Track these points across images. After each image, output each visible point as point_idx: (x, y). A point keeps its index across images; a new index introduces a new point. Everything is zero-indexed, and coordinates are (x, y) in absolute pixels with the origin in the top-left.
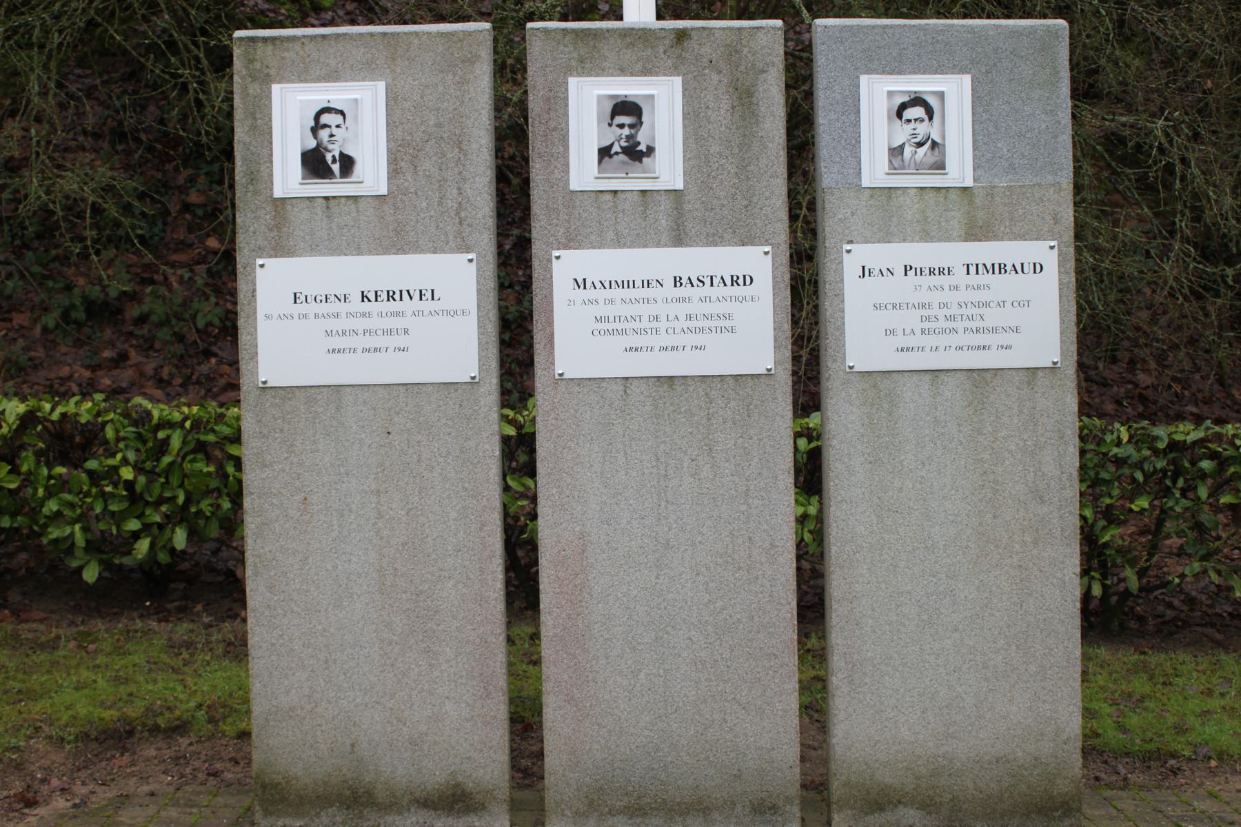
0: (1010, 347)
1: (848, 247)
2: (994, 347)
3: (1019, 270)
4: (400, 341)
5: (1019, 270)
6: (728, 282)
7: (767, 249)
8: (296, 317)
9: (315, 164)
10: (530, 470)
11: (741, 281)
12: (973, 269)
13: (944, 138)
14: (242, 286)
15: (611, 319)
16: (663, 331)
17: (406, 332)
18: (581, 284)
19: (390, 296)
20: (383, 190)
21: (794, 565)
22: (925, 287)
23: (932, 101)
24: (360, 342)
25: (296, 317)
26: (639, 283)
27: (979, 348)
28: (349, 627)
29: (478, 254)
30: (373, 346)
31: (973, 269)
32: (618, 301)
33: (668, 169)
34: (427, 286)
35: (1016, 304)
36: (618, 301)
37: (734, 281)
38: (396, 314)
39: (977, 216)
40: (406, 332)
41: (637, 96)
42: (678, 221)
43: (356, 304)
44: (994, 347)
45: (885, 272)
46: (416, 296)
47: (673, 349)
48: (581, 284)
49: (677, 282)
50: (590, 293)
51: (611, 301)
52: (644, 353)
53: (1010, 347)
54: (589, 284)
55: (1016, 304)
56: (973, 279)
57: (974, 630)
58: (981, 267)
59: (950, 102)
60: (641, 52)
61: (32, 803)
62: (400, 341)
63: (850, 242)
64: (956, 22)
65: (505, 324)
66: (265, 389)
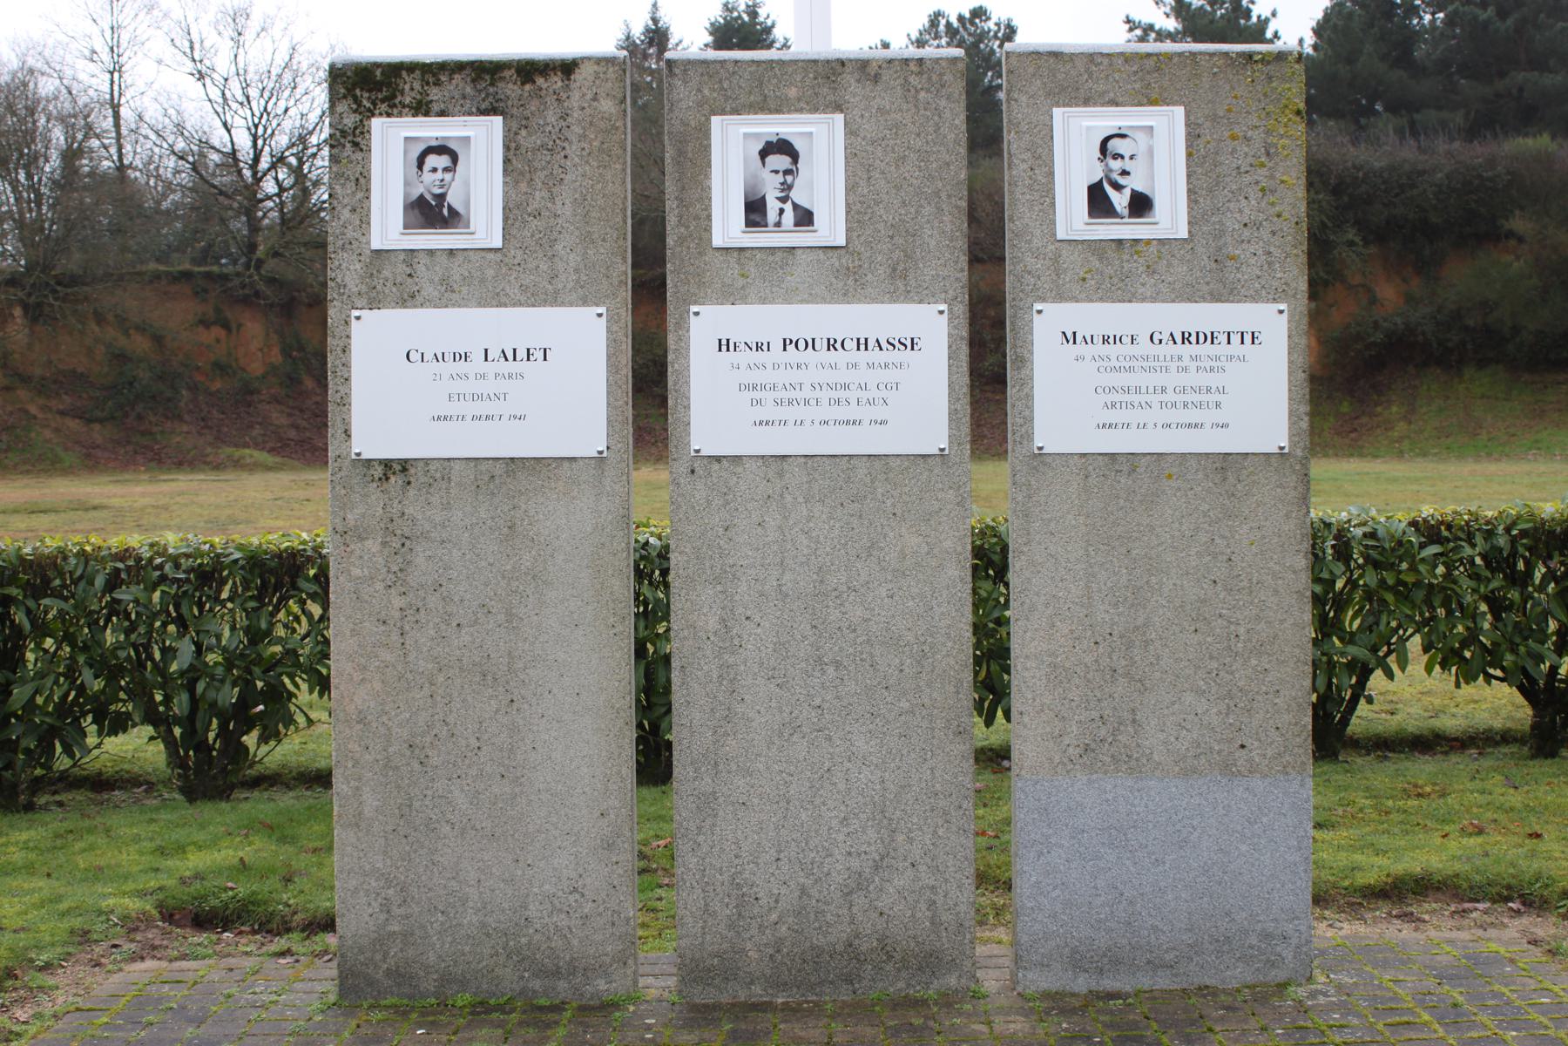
3: (510, 357)
4: (878, 412)
5: (510, 357)
6: (1179, 339)
7: (1283, 307)
8: (472, 377)
9: (1098, 202)
10: (1001, 574)
11: (1193, 339)
12: (1248, 338)
13: (1153, 188)
15: (1144, 390)
16: (854, 402)
17: (1218, 405)
18: (724, 345)
19: (1105, 340)
21: (1308, 653)
22: (446, 376)
23: (798, 145)
25: (472, 377)
26: (522, 354)
27: (848, 422)
28: (463, 780)
29: (950, 310)
30: (484, 414)
31: (1248, 338)
32: (863, 366)
34: (537, 343)
36: (863, 366)
39: (1205, 269)
40: (1218, 405)
43: (1144, 347)
44: (866, 422)
47: (487, 417)
48: (724, 345)
51: (855, 366)
52: (453, 423)
54: (1079, 338)
57: (1177, 817)
59: (1161, 143)
61: (100, 869)
62: (878, 412)
66: (1040, 455)
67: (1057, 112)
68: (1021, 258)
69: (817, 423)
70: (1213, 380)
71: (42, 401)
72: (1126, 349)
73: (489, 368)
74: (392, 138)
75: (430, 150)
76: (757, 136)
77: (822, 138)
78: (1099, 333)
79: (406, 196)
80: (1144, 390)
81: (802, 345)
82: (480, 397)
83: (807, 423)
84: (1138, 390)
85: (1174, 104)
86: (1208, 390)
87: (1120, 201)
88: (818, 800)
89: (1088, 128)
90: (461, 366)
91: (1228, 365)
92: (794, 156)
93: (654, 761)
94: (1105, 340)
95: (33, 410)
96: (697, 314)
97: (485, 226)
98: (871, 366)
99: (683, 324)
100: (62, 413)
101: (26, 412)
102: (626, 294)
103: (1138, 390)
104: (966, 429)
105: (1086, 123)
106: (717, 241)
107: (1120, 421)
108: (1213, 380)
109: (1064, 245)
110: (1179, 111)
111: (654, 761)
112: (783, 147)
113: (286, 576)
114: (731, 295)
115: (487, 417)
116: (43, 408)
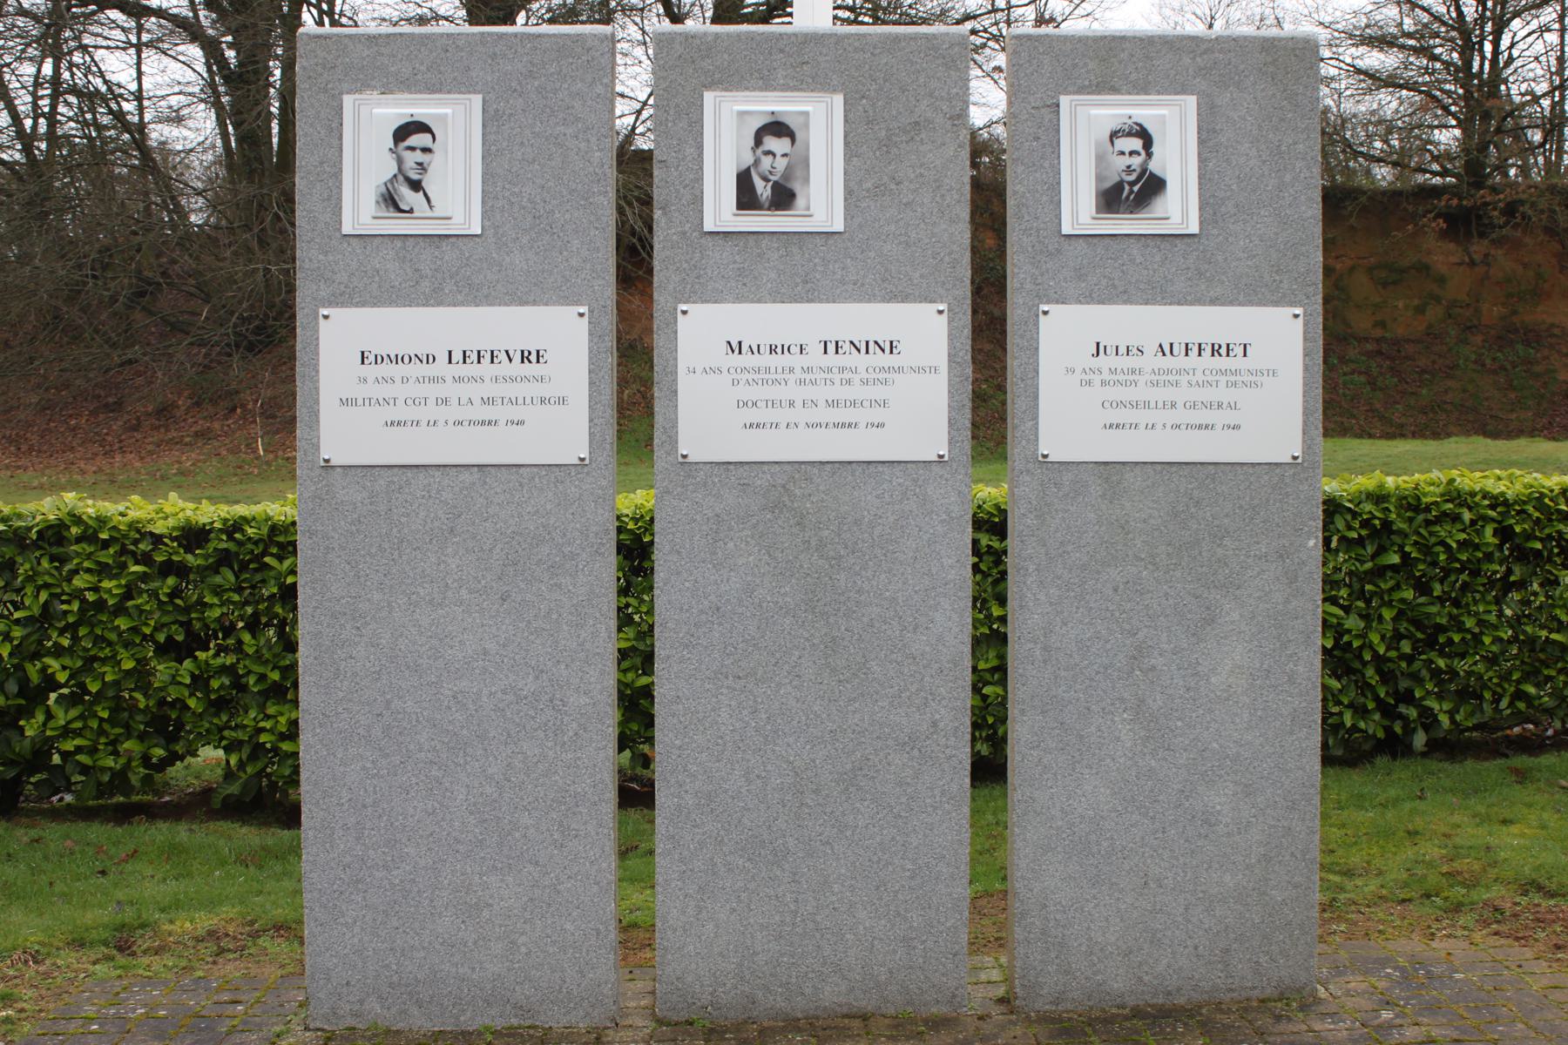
0: (523, 423)
1: (684, 307)
2: (502, 423)
3: (1167, 350)
4: (877, 415)
5: (1167, 350)
7: (1298, 311)
11: (779, 350)
12: (831, 348)
14: (659, 341)
19: (772, 350)
24: (800, 415)
25: (449, 379)
27: (483, 423)
28: (430, 778)
29: (591, 311)
31: (831, 348)
33: (823, 204)
34: (1134, 343)
35: (410, 402)
37: (525, 357)
38: (433, 380)
41: (786, 113)
42: (806, 270)
43: (1151, 361)
50: (747, 360)
52: (408, 429)
53: (523, 423)
54: (745, 348)
55: (410, 402)
56: (832, 359)
60: (808, 63)
62: (877, 415)
63: (1048, 302)
64: (745, 27)
65: (979, 398)
66: (328, 466)
67: (709, 97)
69: (451, 423)
70: (878, 392)
72: (794, 360)
77: (1175, 122)
78: (765, 342)
79: (1099, 178)
80: (1153, 405)
83: (1159, 426)
84: (1147, 405)
87: (763, 190)
89: (742, 114)
91: (1265, 379)
93: (989, 769)
94: (772, 350)
98: (458, 380)
102: (965, 290)
103: (1147, 405)
104: (610, 434)
105: (1094, 111)
106: (347, 228)
107: (768, 420)
108: (878, 392)
109: (354, 241)
110: (1192, 101)
111: (989, 769)
112: (777, 128)
114: (746, 288)
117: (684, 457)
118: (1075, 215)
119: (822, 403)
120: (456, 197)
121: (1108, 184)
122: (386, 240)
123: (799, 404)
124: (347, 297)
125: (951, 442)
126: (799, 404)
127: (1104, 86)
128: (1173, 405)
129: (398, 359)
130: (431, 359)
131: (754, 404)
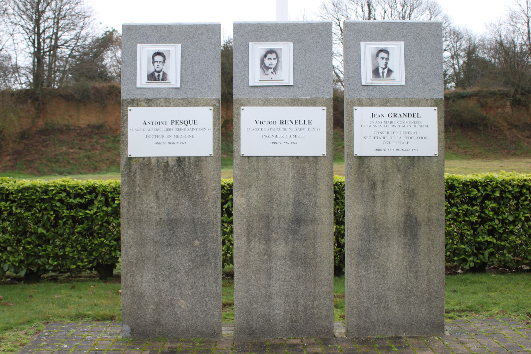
2: (290, 143)
7: (324, 108)
8: (260, 129)
9: (376, 72)
20: (178, 86)
23: (165, 54)
24: (284, 140)
25: (260, 129)
32: (294, 129)
36: (294, 129)
45: (381, 116)
46: (151, 123)
47: (173, 143)
49: (281, 122)
51: (264, 129)
52: (277, 145)
58: (294, 123)
63: (355, 106)
67: (362, 43)
68: (237, 93)
71: (521, 133)
73: (284, 126)
74: (368, 49)
75: (381, 51)
76: (263, 49)
81: (186, 123)
82: (183, 136)
85: (400, 41)
86: (411, 133)
88: (270, 283)
89: (148, 50)
90: (273, 126)
92: (164, 57)
94: (281, 122)
95: (519, 136)
96: (243, 109)
97: (174, 79)
98: (178, 130)
99: (239, 114)
100: (527, 137)
101: (517, 137)
106: (138, 86)
107: (278, 142)
110: (402, 43)
113: (109, 196)
115: (173, 143)
116: (522, 135)
117: (243, 155)
118: (366, 79)
119: (173, 136)
120: (286, 75)
121: (149, 73)
122: (277, 88)
123: (165, 136)
124: (249, 103)
125: (327, 151)
126: (165, 136)
127: (147, 40)
128: (163, 137)
129: (159, 123)
130: (274, 123)
131: (152, 137)
